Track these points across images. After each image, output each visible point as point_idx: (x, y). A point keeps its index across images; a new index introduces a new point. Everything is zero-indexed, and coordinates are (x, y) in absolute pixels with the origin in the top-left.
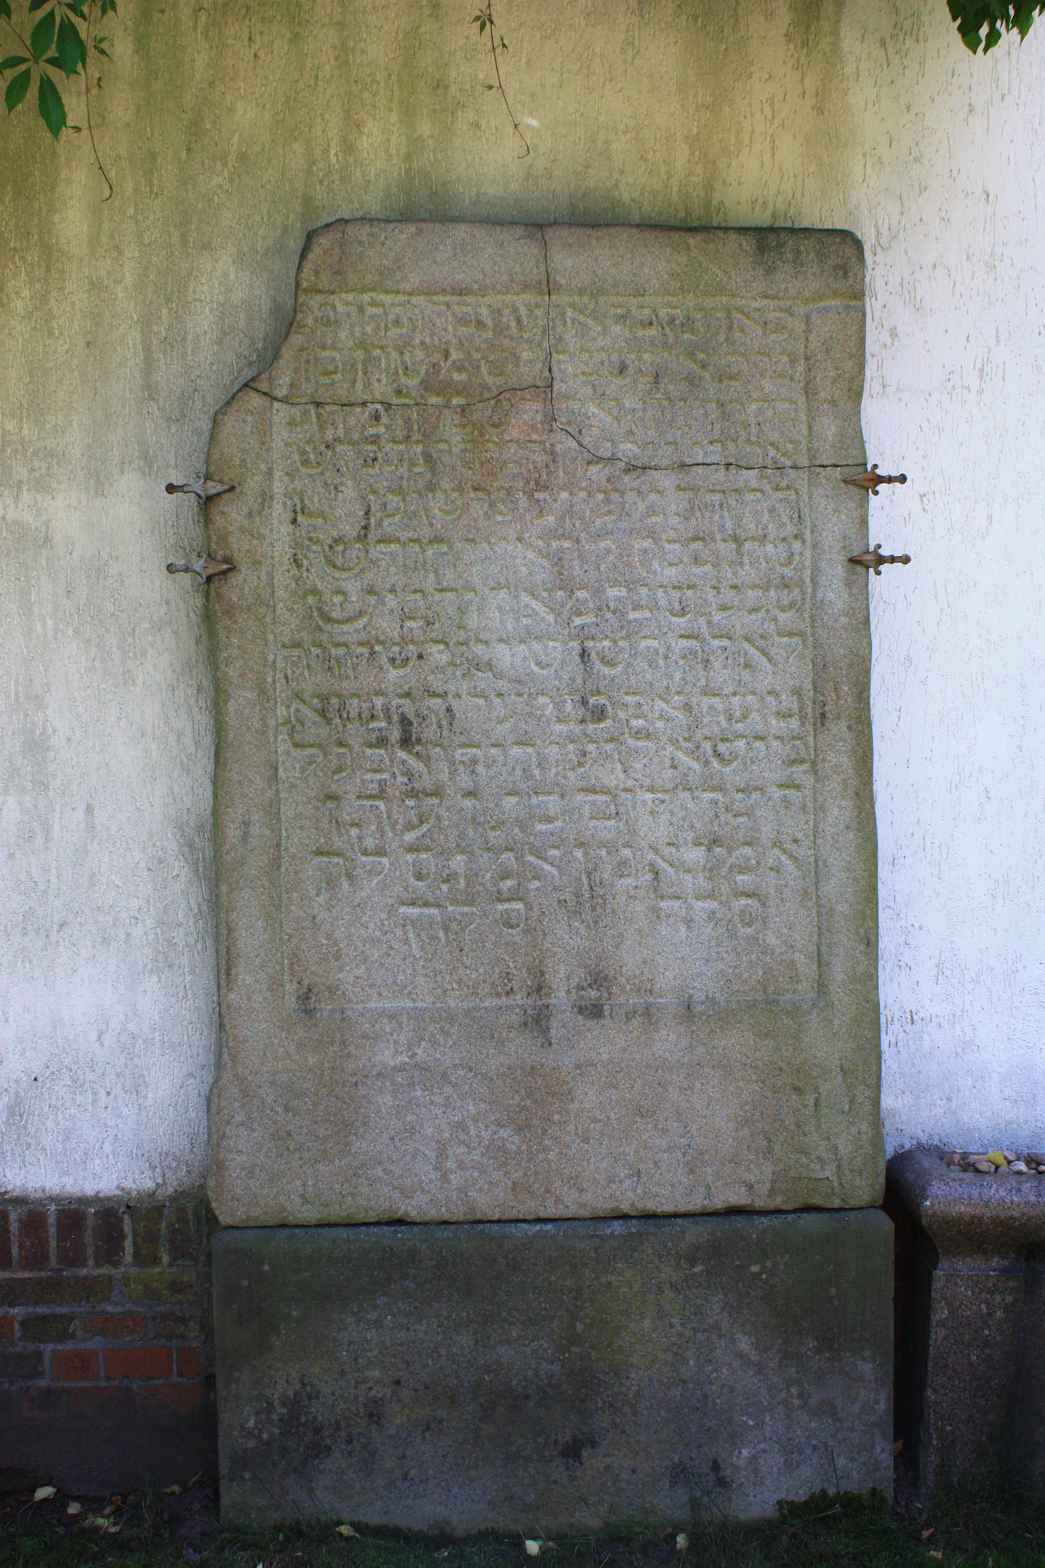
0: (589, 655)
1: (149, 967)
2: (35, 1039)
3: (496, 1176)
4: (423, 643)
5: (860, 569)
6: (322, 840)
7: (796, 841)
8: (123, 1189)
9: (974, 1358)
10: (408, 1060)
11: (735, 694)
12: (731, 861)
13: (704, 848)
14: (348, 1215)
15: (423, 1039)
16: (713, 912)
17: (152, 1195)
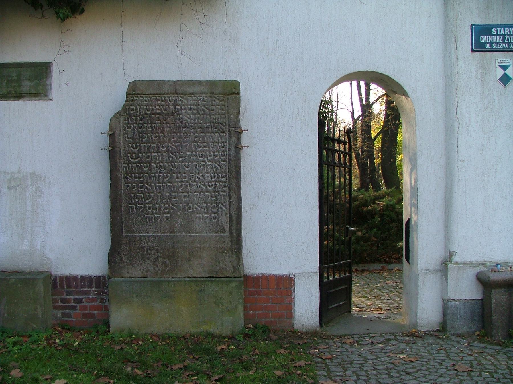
9: (501, 309)
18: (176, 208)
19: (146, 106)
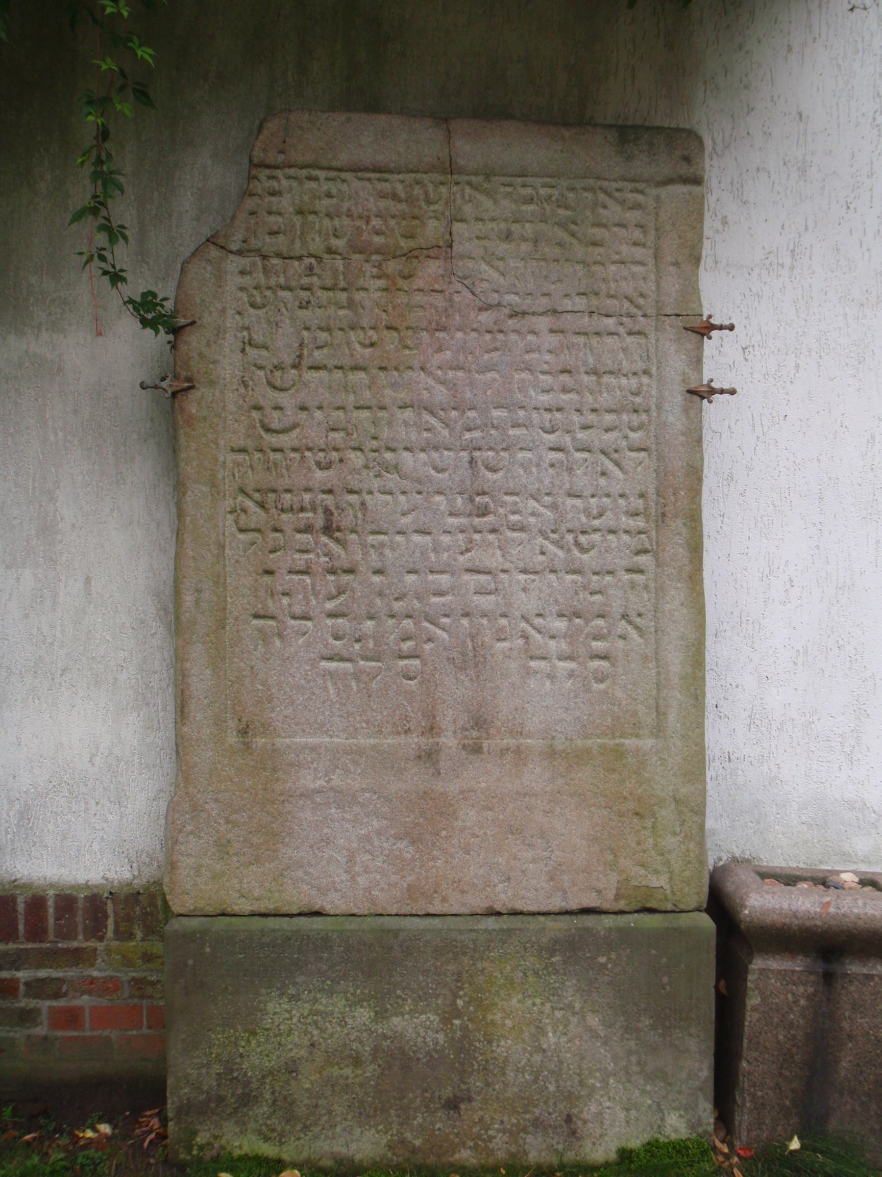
0: (476, 462)
1: (131, 705)
2: (41, 760)
3: (394, 878)
4: (343, 449)
5: (696, 398)
6: (260, 606)
7: (640, 615)
8: (107, 879)
9: (781, 1037)
10: (325, 784)
11: (593, 496)
12: (587, 630)
13: (565, 619)
14: (275, 907)
15: (337, 767)
16: (573, 671)
17: (129, 884)
18: (445, 635)
19: (329, 215)
